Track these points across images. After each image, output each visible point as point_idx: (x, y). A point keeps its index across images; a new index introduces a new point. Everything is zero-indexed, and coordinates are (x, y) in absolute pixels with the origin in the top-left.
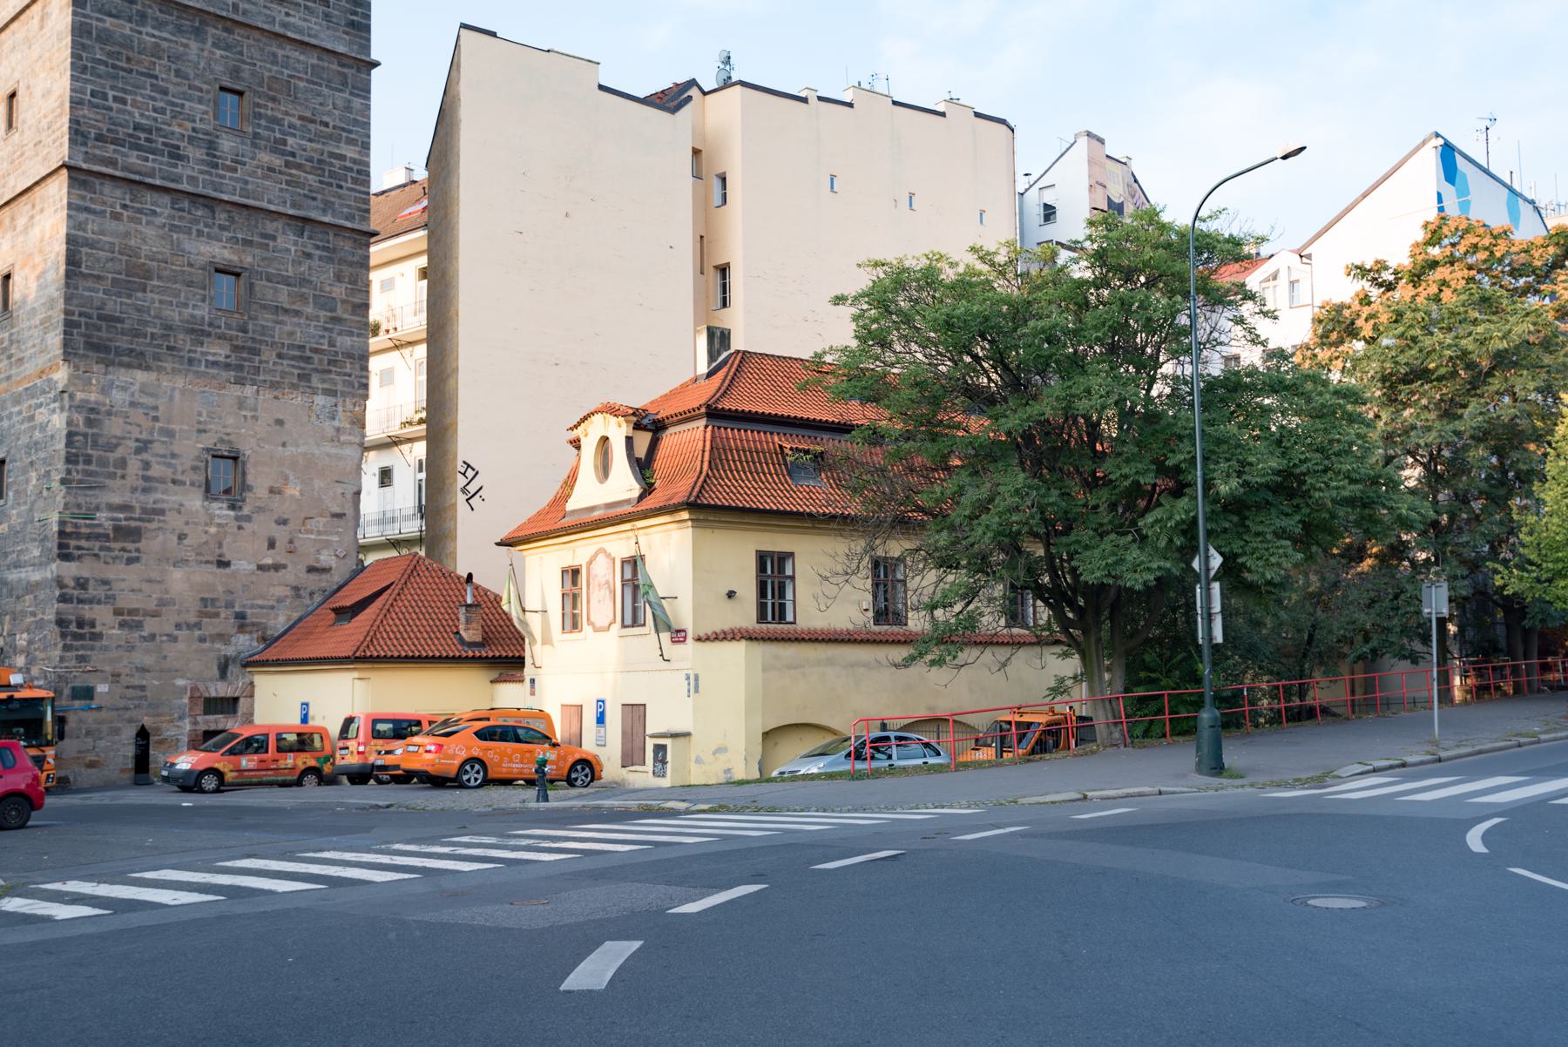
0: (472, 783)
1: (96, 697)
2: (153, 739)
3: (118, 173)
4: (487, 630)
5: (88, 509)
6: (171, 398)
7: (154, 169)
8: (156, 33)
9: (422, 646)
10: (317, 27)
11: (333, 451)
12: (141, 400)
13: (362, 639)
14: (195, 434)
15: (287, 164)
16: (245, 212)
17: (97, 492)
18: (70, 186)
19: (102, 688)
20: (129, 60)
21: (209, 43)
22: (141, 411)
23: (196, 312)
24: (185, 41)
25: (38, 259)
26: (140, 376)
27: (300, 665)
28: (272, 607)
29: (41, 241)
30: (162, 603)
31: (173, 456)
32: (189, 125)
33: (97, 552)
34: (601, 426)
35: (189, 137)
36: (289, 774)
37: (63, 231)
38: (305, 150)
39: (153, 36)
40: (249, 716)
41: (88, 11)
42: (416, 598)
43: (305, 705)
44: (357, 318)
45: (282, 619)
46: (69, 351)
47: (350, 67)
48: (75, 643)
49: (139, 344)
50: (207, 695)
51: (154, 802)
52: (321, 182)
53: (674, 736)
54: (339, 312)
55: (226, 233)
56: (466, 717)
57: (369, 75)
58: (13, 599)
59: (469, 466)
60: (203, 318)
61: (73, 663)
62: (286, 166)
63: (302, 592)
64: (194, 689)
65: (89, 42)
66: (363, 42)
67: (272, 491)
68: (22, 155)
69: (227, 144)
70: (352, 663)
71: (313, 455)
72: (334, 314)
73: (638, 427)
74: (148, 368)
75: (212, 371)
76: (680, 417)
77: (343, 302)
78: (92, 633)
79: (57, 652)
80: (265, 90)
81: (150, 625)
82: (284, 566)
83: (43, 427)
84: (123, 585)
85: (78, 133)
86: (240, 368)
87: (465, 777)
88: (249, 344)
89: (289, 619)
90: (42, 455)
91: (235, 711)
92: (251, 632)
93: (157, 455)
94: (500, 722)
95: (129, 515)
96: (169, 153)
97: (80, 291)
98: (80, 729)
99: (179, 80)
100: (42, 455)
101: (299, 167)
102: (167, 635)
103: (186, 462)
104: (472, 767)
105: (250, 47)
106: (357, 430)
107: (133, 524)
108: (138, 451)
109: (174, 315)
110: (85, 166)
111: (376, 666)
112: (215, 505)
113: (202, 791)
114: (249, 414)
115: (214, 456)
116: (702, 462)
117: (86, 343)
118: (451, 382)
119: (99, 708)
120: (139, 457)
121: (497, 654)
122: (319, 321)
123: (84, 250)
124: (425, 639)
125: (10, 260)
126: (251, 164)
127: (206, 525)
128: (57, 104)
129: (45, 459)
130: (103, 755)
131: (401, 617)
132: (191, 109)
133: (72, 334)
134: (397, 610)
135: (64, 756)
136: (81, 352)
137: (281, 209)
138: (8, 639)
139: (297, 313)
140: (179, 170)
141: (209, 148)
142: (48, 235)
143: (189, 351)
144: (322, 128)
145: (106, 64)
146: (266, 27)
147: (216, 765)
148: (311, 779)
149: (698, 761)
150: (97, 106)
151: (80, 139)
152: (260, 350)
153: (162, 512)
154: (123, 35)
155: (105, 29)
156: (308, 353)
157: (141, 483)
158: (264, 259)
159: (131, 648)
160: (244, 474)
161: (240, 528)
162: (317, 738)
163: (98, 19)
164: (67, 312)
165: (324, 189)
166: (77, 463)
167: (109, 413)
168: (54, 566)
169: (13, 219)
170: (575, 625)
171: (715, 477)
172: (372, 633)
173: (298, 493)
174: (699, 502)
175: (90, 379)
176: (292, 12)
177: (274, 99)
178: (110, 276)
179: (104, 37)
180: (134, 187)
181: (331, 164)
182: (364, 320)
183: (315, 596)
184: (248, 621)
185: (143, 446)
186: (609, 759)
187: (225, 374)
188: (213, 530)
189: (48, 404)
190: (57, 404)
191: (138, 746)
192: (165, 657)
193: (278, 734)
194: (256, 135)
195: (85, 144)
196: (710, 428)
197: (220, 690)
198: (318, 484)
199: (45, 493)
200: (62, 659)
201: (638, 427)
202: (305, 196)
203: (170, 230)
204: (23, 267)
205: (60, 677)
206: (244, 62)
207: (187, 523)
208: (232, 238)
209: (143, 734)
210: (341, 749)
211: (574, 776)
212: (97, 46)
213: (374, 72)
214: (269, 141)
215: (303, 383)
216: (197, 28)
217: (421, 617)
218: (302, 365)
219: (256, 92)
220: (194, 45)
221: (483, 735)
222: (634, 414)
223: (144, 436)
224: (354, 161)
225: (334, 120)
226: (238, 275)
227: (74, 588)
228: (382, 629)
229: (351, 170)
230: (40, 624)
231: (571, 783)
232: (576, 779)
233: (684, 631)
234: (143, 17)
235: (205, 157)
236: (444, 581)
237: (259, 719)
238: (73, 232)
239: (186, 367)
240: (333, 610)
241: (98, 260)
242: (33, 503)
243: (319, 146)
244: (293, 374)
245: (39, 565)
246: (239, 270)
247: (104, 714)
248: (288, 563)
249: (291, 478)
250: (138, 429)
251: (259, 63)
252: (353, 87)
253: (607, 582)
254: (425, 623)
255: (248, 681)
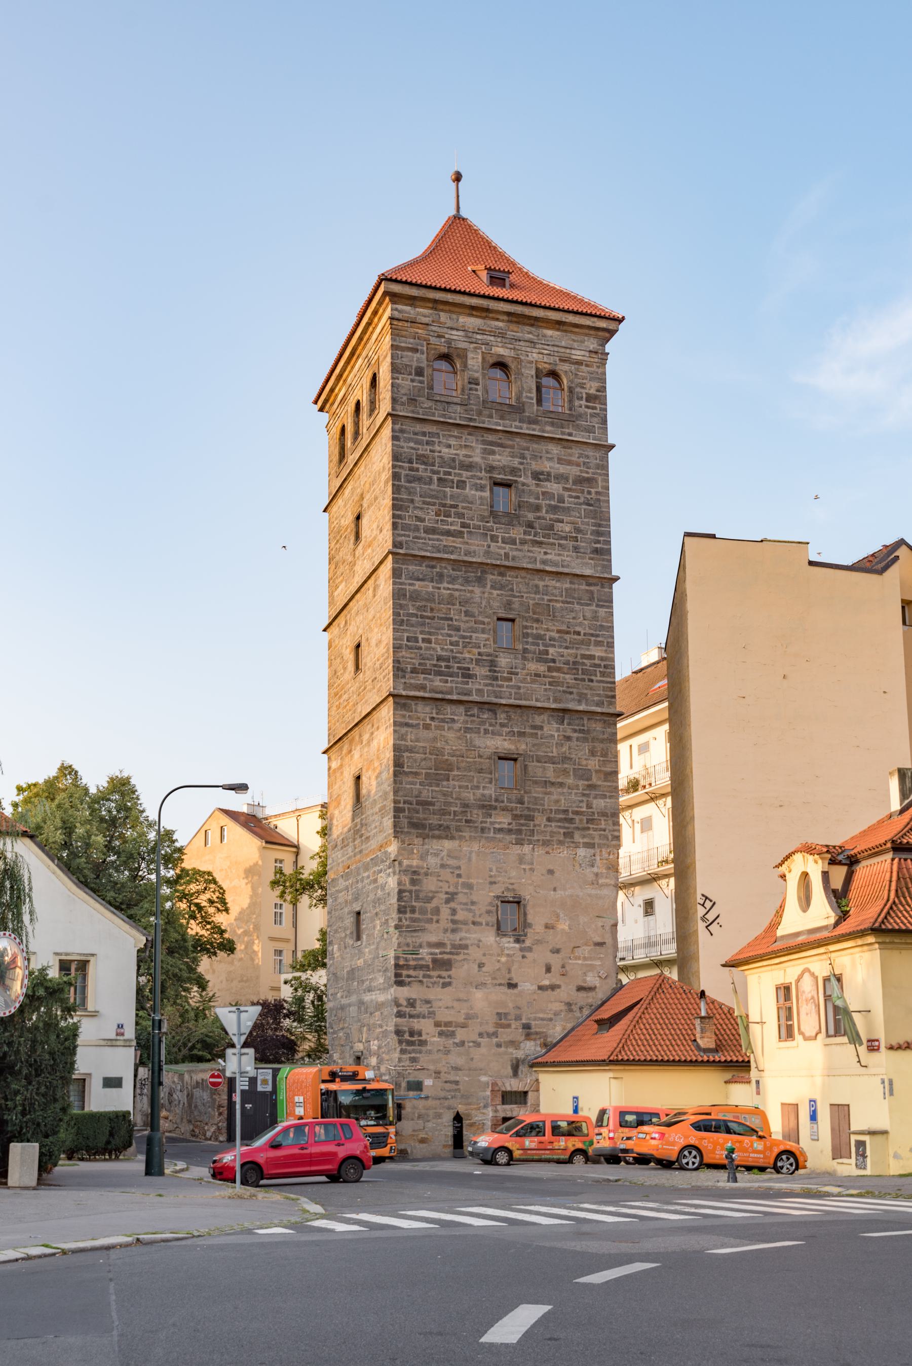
0: (690, 1166)
1: (424, 1089)
2: (465, 1122)
3: (427, 695)
4: (721, 1038)
5: (414, 947)
6: (470, 859)
7: (452, 687)
8: (450, 586)
9: (664, 1051)
10: (568, 559)
11: (593, 892)
12: (448, 863)
13: (615, 1045)
14: (488, 886)
15: (550, 669)
16: (519, 711)
17: (420, 934)
18: (395, 709)
19: (428, 1082)
20: (432, 610)
21: (489, 586)
22: (448, 870)
23: (486, 792)
24: (470, 588)
25: (376, 764)
26: (447, 844)
27: (569, 1066)
28: (551, 1020)
29: (378, 750)
30: (468, 1017)
31: (473, 903)
32: (476, 651)
33: (421, 979)
34: (804, 863)
35: (476, 660)
36: (562, 1154)
37: (391, 742)
38: (562, 656)
39: (449, 589)
40: (536, 1108)
41: (403, 580)
42: (661, 1011)
43: (576, 1099)
44: (609, 784)
45: (558, 1029)
46: (398, 831)
47: (595, 585)
48: (408, 1048)
49: (446, 820)
50: (504, 1089)
51: (457, 1170)
52: (576, 679)
53: (872, 1133)
54: (594, 780)
55: (505, 729)
56: (690, 1111)
57: (611, 588)
58: (368, 1015)
59: (707, 898)
60: (491, 796)
61: (407, 1063)
62: (549, 671)
63: (573, 1007)
64: (494, 1084)
65: (405, 602)
66: (605, 563)
67: (547, 927)
68: (365, 688)
69: (504, 661)
70: (607, 1065)
71: (578, 896)
72: (590, 783)
73: (833, 862)
74: (452, 838)
75: (498, 836)
76: (869, 852)
77: (597, 771)
78: (420, 1041)
79: (396, 1055)
80: (531, 614)
81: (461, 1034)
82: (559, 987)
83: (383, 888)
84: (440, 1004)
85: (399, 670)
86: (519, 832)
87: (684, 1161)
88: (526, 812)
89: (564, 1029)
90: (383, 907)
91: (525, 1103)
92: (535, 1040)
93: (461, 903)
94: (720, 1117)
95: (443, 950)
96: (462, 674)
97: (404, 785)
98: (414, 1113)
99: (467, 618)
100: (383, 907)
101: (559, 670)
102: (473, 1042)
103: (482, 907)
104: (690, 1153)
105: (517, 582)
106: (612, 874)
107: (446, 957)
108: (448, 901)
109: (470, 796)
110: (404, 693)
111: (627, 1068)
112: (505, 940)
113: (497, 1164)
114: (527, 867)
115: (502, 902)
116: (889, 891)
117: (409, 823)
118: (690, 828)
119: (427, 1098)
120: (448, 906)
121: (729, 1059)
122: (578, 789)
123: (406, 754)
124: (667, 1046)
125: (360, 766)
126: (522, 673)
127: (499, 955)
128: (384, 650)
129: (384, 911)
130: (430, 1134)
131: (648, 1027)
132: (477, 638)
133: (399, 818)
134: (645, 1021)
135: (404, 1134)
136: (406, 830)
137: (546, 705)
138: (366, 1045)
139: (561, 785)
140: (470, 686)
141: (491, 666)
142: (382, 746)
143: (482, 822)
144: (576, 637)
145: (416, 616)
146: (530, 566)
147: (507, 1145)
148: (579, 1158)
149: (896, 1156)
150: (411, 648)
151: (400, 673)
152: (534, 816)
153: (466, 947)
154: (427, 592)
155: (415, 591)
156: (571, 816)
157: (450, 925)
158: (534, 745)
159: (447, 1052)
160: (525, 914)
161: (523, 957)
162: (584, 1124)
163: (410, 584)
164: (395, 802)
165: (578, 684)
166: (405, 912)
167: (426, 874)
168: (392, 990)
169: (360, 736)
170: (790, 1035)
171: (901, 903)
172: (623, 1041)
173: (567, 928)
174: (883, 927)
175: (413, 850)
176: (549, 551)
177: (537, 621)
178: (424, 771)
179: (415, 597)
180: (439, 703)
181: (583, 664)
182: (614, 784)
183: (584, 1010)
184: (532, 1030)
185: (451, 897)
186: (822, 1152)
187: (508, 837)
188: (503, 959)
189: (385, 870)
190: (391, 870)
191: (455, 1127)
192: (472, 1059)
193: (552, 1121)
194: (525, 651)
195: (404, 677)
196: (896, 860)
197: (513, 1085)
198: (583, 919)
199: (385, 936)
200: (400, 1060)
201: (833, 862)
202: (564, 692)
203: (465, 732)
204: (367, 770)
205: (399, 1073)
206: (515, 596)
207: (484, 955)
208: (510, 732)
209: (458, 1118)
210: (597, 1134)
211: (779, 1164)
212: (410, 604)
213: (615, 586)
214: (534, 653)
215: (568, 840)
216: (480, 577)
217: (665, 1027)
218: (567, 825)
219: (524, 617)
220: (477, 590)
221: (698, 1126)
222: (828, 852)
223: (452, 890)
224: (602, 659)
225: (585, 629)
226: (515, 760)
227: (406, 1007)
228: (631, 1037)
229: (599, 666)
230: (385, 1034)
231: (778, 1170)
232: (782, 1167)
233: (877, 1040)
234: (441, 576)
235: (488, 673)
236: (684, 996)
237: (544, 1109)
238: (398, 742)
239: (479, 834)
240: (596, 1021)
241: (415, 761)
242: (378, 943)
243: (574, 651)
244: (559, 833)
245: (384, 990)
246: (515, 756)
247: (430, 1102)
248: (562, 984)
249: (562, 915)
250: (447, 885)
251: (525, 595)
252: (598, 600)
253: (813, 998)
254: (668, 1032)
255: (534, 1078)
